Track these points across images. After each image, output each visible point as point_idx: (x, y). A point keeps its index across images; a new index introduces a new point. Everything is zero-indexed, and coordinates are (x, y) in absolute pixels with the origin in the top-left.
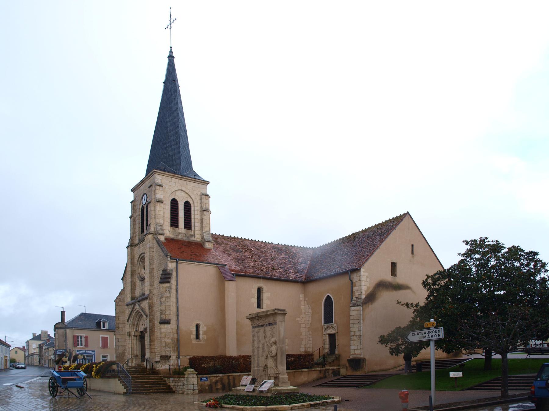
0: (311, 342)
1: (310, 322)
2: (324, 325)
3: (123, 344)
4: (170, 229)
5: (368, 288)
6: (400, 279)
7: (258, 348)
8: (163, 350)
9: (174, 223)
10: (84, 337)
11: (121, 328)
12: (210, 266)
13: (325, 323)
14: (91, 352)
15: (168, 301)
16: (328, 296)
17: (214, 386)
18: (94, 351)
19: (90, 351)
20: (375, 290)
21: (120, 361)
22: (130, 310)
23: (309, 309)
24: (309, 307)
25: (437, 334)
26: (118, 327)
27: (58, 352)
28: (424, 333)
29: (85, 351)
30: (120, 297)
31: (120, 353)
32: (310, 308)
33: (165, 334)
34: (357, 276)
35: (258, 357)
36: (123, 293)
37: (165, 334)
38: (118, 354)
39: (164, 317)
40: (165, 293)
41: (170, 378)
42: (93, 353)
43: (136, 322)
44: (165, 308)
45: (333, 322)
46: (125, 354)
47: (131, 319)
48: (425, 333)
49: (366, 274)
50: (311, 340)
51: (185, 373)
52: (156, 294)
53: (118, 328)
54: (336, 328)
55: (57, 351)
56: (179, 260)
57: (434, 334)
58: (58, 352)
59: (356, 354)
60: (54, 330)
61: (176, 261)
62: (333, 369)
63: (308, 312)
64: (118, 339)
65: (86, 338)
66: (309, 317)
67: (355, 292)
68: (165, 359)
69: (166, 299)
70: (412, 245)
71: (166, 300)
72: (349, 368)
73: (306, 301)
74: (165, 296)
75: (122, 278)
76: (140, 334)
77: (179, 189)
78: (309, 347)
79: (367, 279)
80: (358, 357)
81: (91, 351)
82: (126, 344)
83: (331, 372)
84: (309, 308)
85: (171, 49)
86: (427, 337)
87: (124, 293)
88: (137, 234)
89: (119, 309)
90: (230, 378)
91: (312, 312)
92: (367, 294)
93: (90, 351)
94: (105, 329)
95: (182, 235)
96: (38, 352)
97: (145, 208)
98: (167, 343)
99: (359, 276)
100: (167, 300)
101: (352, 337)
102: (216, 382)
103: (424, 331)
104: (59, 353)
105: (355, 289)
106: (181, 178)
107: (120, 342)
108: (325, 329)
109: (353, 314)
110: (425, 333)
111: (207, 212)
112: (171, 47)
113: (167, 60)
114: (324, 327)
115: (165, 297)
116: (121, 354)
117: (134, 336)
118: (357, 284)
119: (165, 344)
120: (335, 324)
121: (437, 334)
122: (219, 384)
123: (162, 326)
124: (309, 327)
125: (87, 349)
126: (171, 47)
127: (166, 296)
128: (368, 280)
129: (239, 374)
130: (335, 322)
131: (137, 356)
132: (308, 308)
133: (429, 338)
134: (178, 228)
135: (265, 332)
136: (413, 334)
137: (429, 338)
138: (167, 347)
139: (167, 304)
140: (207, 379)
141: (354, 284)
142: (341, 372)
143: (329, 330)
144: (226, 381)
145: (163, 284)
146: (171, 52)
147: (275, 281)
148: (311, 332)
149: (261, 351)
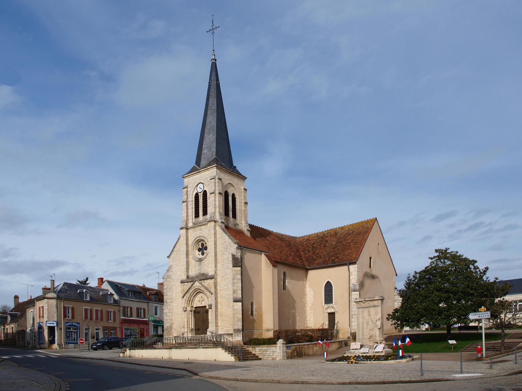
3: (171, 318)
7: (363, 323)
10: (71, 308)
12: (259, 253)
14: (76, 324)
18: (79, 323)
19: (76, 323)
20: (363, 279)
22: (189, 286)
23: (311, 292)
24: (311, 290)
25: (487, 315)
27: (49, 324)
28: (479, 314)
29: (72, 323)
30: (168, 274)
32: (312, 290)
34: (353, 267)
35: (363, 329)
36: (171, 270)
41: (256, 348)
42: (78, 325)
44: (237, 288)
45: (332, 303)
46: (173, 327)
47: (188, 295)
48: (480, 314)
53: (166, 303)
55: (47, 323)
56: (243, 247)
57: (485, 315)
58: (49, 324)
61: (240, 247)
63: (310, 294)
64: (167, 313)
65: (73, 309)
66: (311, 298)
67: (352, 280)
68: (237, 332)
69: (238, 280)
71: (237, 281)
74: (236, 278)
77: (198, 183)
78: (311, 323)
81: (77, 323)
84: (311, 291)
86: (481, 317)
93: (76, 323)
94: (87, 301)
97: (201, 196)
98: (239, 318)
100: (238, 282)
101: (353, 316)
103: (479, 313)
104: (49, 325)
106: (231, 173)
109: (353, 298)
110: (480, 314)
115: (237, 279)
117: (191, 311)
120: (335, 304)
121: (487, 315)
124: (311, 307)
125: (73, 321)
127: (238, 278)
132: (310, 290)
133: (482, 317)
134: (229, 216)
135: (369, 312)
136: (472, 315)
137: (482, 317)
138: (238, 322)
143: (329, 309)
148: (312, 311)
149: (366, 324)
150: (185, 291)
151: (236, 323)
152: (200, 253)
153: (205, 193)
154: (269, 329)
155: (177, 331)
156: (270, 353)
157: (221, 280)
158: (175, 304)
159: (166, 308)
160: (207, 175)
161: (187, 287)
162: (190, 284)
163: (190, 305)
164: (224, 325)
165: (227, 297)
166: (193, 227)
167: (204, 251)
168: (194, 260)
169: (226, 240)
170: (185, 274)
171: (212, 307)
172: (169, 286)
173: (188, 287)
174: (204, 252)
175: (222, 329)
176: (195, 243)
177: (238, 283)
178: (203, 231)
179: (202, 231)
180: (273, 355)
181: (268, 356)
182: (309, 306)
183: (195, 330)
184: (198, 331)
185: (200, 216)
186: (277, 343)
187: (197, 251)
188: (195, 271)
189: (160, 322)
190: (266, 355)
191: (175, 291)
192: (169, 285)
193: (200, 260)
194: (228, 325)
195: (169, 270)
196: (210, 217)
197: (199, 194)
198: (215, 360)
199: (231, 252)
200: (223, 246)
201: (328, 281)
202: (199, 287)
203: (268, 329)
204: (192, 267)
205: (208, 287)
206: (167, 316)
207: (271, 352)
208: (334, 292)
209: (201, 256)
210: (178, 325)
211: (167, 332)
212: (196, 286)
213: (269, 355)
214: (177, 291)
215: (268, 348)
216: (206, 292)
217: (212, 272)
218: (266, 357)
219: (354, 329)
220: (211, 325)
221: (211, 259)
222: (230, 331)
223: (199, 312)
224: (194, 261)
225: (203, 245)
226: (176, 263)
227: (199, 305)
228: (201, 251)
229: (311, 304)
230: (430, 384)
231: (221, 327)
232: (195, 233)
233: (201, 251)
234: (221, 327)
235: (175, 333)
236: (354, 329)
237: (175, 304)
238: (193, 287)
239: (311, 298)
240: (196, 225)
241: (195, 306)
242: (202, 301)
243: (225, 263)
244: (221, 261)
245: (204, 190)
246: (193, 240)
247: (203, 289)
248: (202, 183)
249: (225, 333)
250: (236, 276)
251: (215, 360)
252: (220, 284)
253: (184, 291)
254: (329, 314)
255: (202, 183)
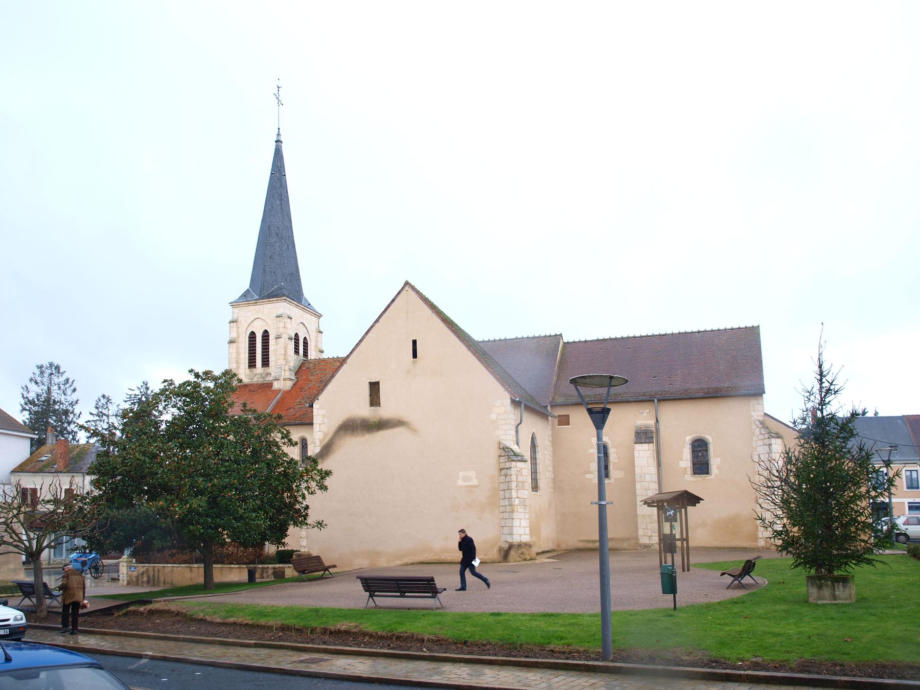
4: (248, 371)
5: (325, 435)
6: (386, 410)
9: (252, 364)
17: (140, 577)
49: (322, 412)
60: (686, 492)
62: (274, 568)
70: (414, 342)
79: (323, 421)
83: (270, 572)
85: (279, 132)
90: (156, 569)
92: (322, 445)
95: (258, 376)
96: (598, 538)
102: (143, 573)
111: (280, 339)
112: (279, 129)
113: (273, 146)
122: (145, 575)
128: (325, 421)
129: (163, 565)
140: (135, 569)
142: (286, 573)
144: (151, 573)
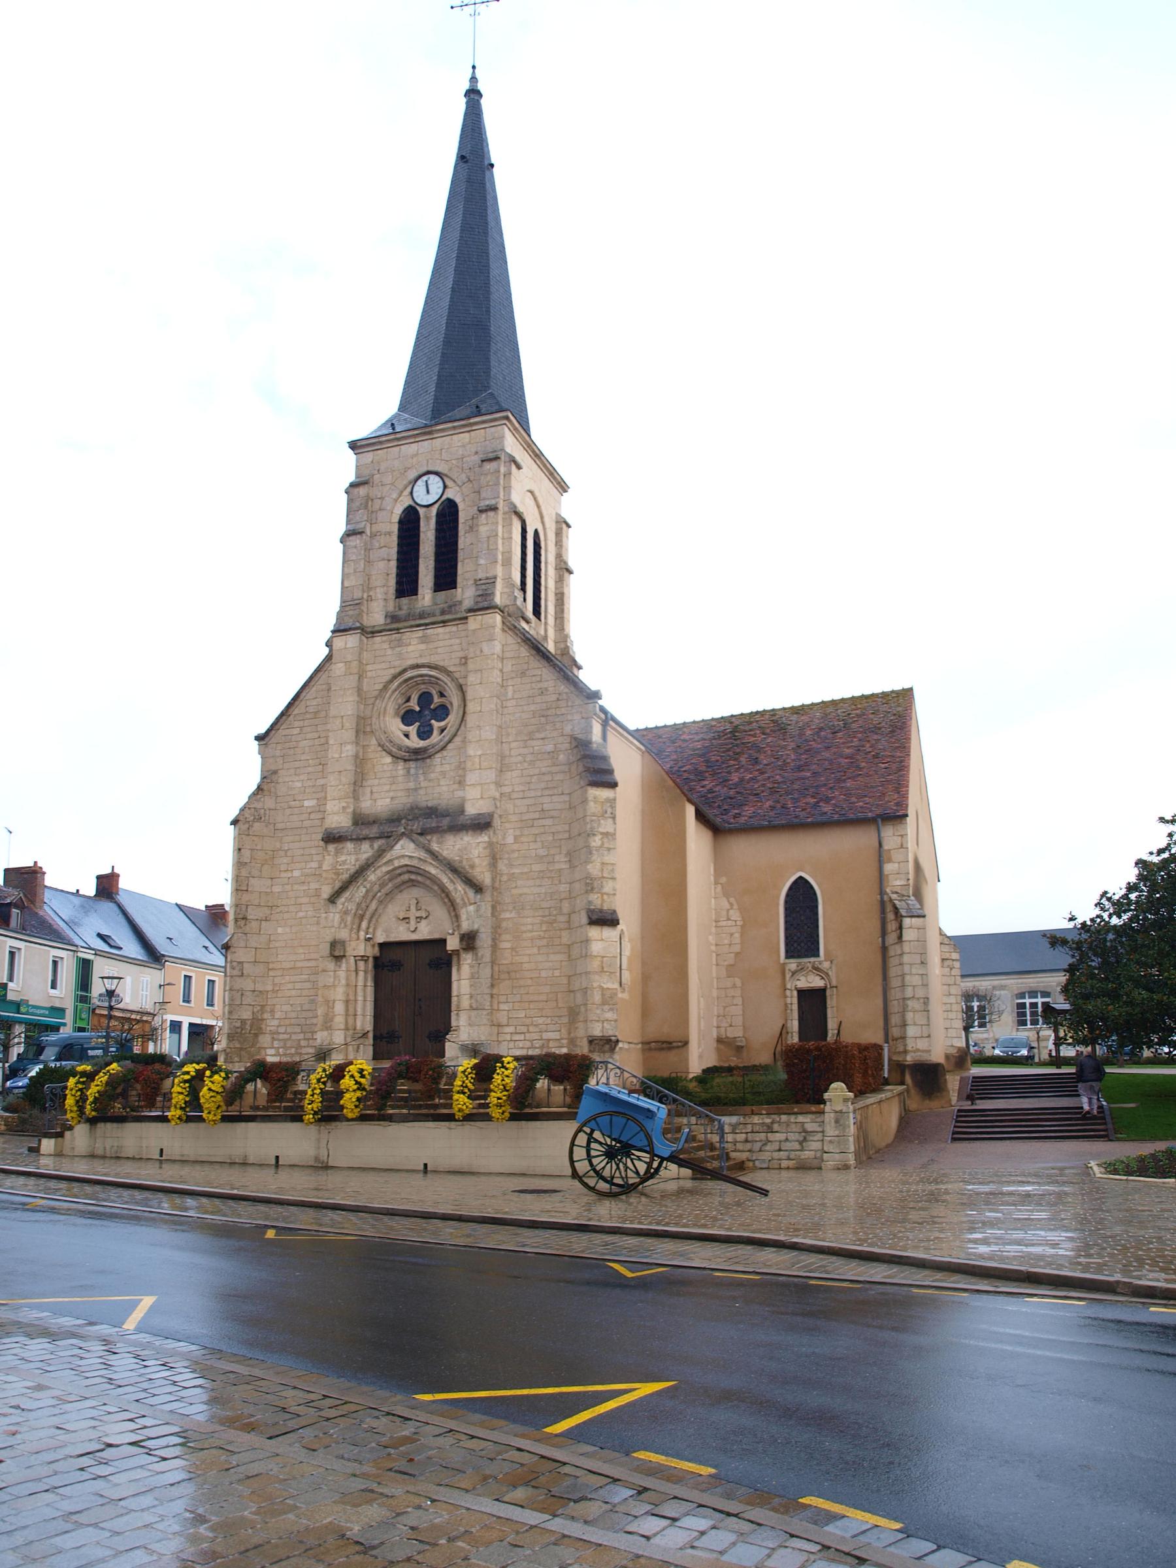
0: (738, 1010)
1: (737, 948)
2: (787, 961)
3: (259, 987)
8: (594, 1018)
11: (254, 924)
13: (789, 955)
15: (609, 849)
16: (802, 884)
21: (243, 1053)
23: (731, 912)
24: (731, 905)
26: (245, 918)
30: (258, 805)
31: (243, 1022)
33: (602, 962)
36: (270, 791)
37: (602, 962)
38: (238, 1024)
39: (596, 900)
40: (602, 821)
43: (373, 906)
45: (818, 956)
47: (358, 892)
50: (740, 1003)
51: (342, 1102)
52: (513, 818)
53: (243, 922)
54: (830, 973)
59: (918, 1050)
63: (728, 919)
64: (242, 963)
66: (732, 935)
69: (605, 840)
71: (603, 844)
72: (913, 1091)
73: (719, 887)
74: (601, 830)
75: (263, 731)
76: (378, 954)
77: (420, 472)
78: (731, 1026)
80: (922, 1059)
82: (269, 988)
87: (273, 789)
88: (379, 593)
89: (252, 850)
91: (743, 919)
97: (428, 518)
98: (608, 994)
99: (902, 836)
100: (606, 845)
105: (889, 868)
107: (248, 976)
108: (794, 973)
112: (474, 67)
114: (787, 969)
115: (602, 833)
116: (248, 1027)
118: (896, 856)
119: (603, 995)
120: (826, 960)
123: (594, 932)
126: (474, 67)
130: (825, 955)
131: (365, 1035)
132: (727, 906)
139: (608, 858)
141: (885, 857)
145: (595, 788)
146: (473, 79)
147: (643, 812)
148: (738, 982)
150: (345, 876)
151: (598, 1012)
152: (413, 730)
153: (448, 513)
154: (670, 1043)
155: (285, 1040)
156: (787, 1140)
157: (516, 837)
158: (280, 930)
159: (242, 944)
160: (464, 446)
161: (353, 858)
162: (366, 851)
163: (362, 934)
164: (528, 1021)
165: (545, 905)
166: (388, 627)
167: (433, 722)
168: (390, 753)
169: (545, 685)
170: (348, 807)
171: (478, 943)
172: (260, 853)
173: (357, 860)
174: (431, 726)
175: (516, 1037)
176: (396, 690)
177: (606, 853)
178: (435, 645)
179: (431, 646)
180: (802, 1150)
181: (777, 1153)
182: (726, 963)
183: (375, 1038)
184: (388, 1042)
185: (420, 591)
186: (826, 1096)
187: (399, 721)
188: (392, 798)
189: (23, 1009)
190: (768, 1148)
191: (283, 875)
192: (259, 847)
193: (418, 756)
194: (549, 1021)
195: (265, 787)
196: (480, 593)
197: (421, 511)
198: (426, 1165)
199: (568, 729)
200: (532, 707)
201: (801, 878)
202: (415, 863)
203: (663, 1042)
204: (376, 782)
205: (461, 862)
206: (242, 975)
207: (792, 1136)
208: (3, 971)
209: (415, 742)
210: (294, 1015)
211: (238, 1046)
212: (403, 856)
213: (780, 1150)
214: (296, 873)
215: (776, 1117)
216: (452, 881)
217: (481, 802)
218: (766, 1156)
219: (914, 1052)
220: (470, 1018)
221: (479, 753)
222: (557, 1044)
223: (396, 966)
224: (389, 759)
225: (425, 698)
226: (297, 764)
227: (402, 934)
228: (417, 724)
229: (732, 955)
230: (590, 1220)
231: (511, 1029)
232: (398, 649)
233: (417, 724)
234: (511, 1029)
235: (271, 1052)
236: (914, 1052)
237: (280, 930)
238: (385, 860)
239: (732, 935)
240: (396, 623)
241: (381, 938)
242: (421, 918)
243: (537, 771)
244: (521, 763)
245: (444, 497)
246: (388, 678)
247: (433, 871)
248: (436, 473)
249: (530, 1053)
250: (599, 825)
251: (426, 1165)
252: (513, 851)
253: (338, 874)
254: (803, 994)
255: (436, 473)
